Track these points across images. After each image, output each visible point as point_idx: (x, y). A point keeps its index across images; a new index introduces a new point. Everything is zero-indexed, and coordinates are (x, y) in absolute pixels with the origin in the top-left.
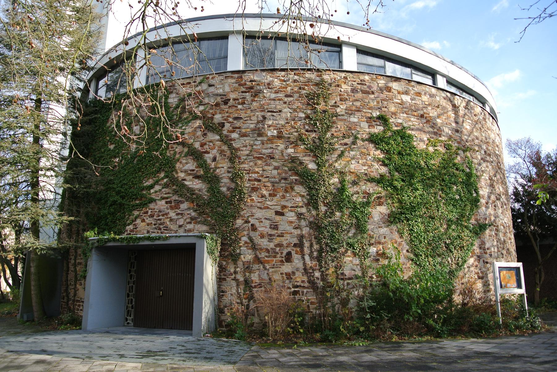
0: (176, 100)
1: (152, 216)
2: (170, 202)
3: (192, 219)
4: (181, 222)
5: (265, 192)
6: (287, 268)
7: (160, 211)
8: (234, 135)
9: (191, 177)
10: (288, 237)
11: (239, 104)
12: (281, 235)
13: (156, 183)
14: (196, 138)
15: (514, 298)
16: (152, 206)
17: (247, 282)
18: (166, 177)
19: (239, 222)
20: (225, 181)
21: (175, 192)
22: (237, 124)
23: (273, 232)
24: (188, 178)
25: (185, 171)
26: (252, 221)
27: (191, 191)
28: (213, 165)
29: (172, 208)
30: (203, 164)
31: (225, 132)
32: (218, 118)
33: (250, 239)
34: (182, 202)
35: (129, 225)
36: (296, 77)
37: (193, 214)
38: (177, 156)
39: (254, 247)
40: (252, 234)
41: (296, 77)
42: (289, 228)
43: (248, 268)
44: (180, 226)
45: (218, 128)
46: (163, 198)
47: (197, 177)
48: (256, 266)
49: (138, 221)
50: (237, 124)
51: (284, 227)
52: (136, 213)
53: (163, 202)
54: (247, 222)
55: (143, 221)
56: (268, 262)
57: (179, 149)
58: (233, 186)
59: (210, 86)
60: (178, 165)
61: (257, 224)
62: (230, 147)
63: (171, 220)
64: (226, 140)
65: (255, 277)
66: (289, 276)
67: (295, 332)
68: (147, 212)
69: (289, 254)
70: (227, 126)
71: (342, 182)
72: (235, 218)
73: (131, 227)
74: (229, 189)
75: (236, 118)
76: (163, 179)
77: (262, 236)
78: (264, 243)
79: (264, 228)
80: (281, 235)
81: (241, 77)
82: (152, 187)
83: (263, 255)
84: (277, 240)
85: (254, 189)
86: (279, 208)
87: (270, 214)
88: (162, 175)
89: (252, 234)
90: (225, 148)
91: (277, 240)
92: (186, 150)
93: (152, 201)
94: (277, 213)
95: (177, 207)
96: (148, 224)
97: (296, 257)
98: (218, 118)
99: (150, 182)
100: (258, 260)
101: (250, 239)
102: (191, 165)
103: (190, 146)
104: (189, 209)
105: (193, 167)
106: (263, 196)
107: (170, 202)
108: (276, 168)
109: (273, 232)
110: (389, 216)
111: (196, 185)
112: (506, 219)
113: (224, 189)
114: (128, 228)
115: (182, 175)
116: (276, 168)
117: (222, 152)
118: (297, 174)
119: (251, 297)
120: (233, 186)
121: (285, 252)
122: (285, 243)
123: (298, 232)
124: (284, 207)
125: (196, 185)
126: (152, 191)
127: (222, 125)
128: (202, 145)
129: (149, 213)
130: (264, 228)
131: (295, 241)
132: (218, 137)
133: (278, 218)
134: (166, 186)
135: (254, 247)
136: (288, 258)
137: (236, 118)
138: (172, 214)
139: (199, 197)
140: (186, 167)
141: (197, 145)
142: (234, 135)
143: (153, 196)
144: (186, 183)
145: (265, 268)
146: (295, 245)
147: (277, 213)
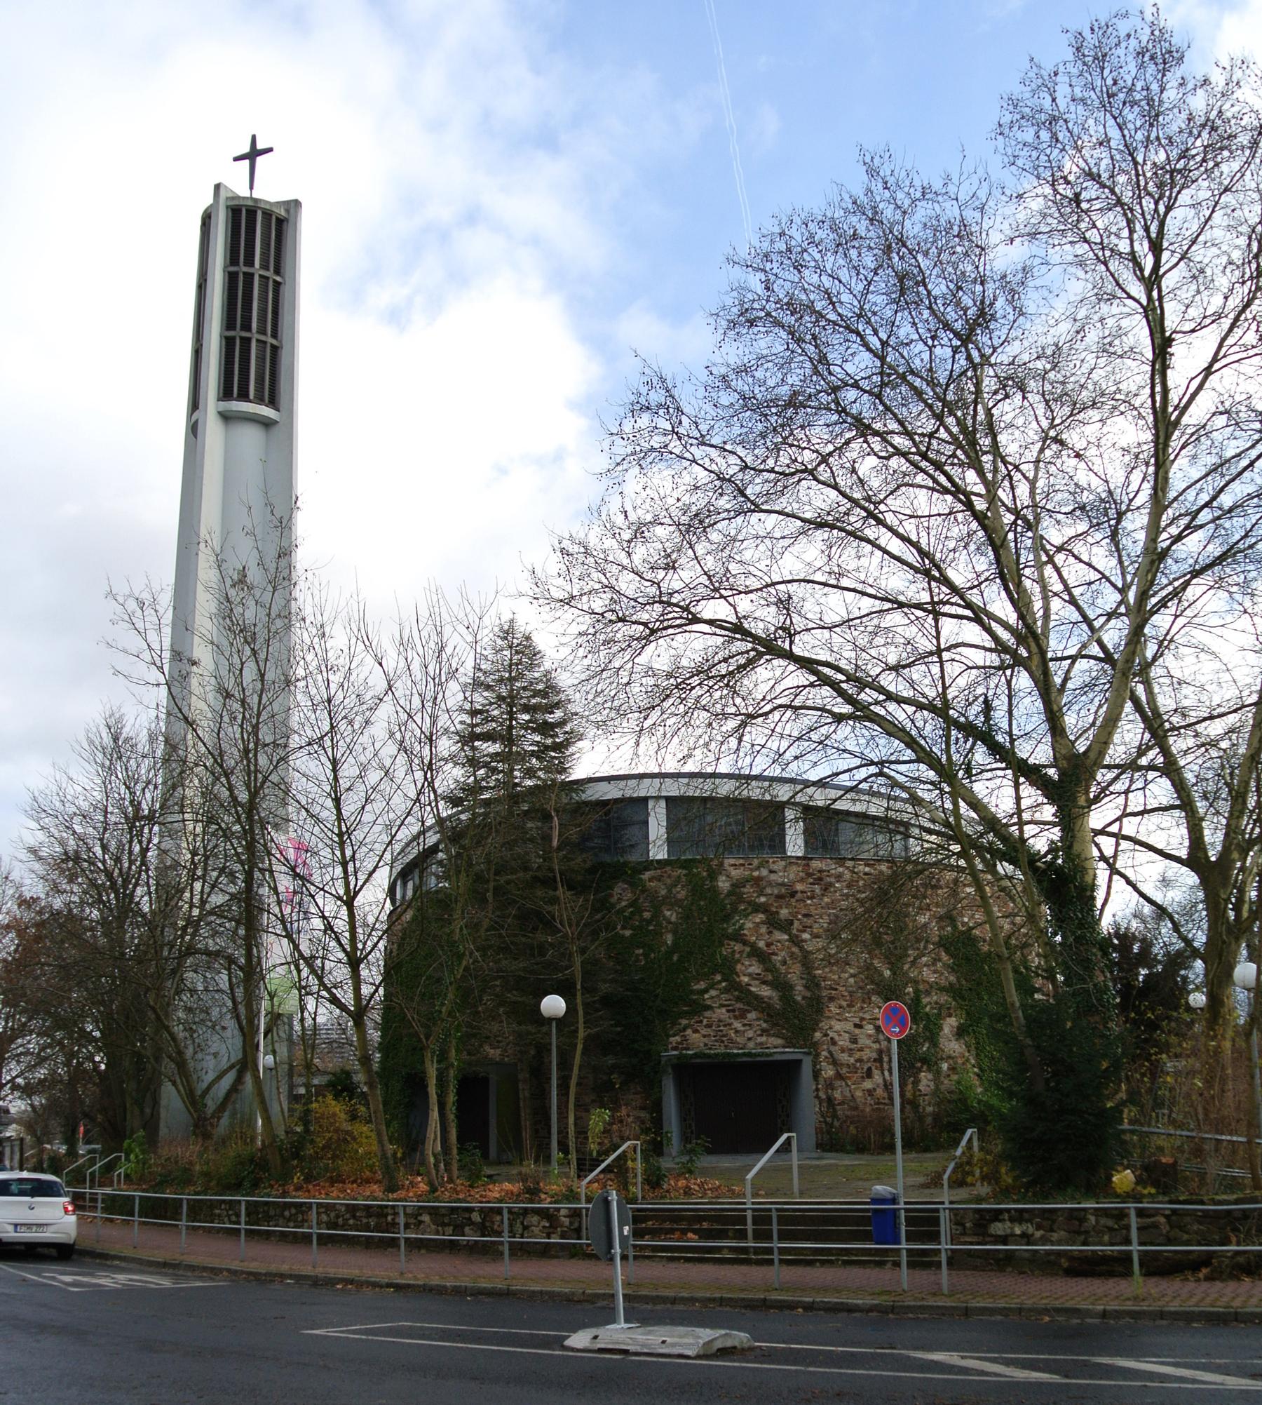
0: (727, 884)
1: (708, 1026)
2: (733, 1011)
3: (764, 1031)
4: (750, 1034)
5: (844, 1004)
6: (868, 1084)
7: (720, 1021)
8: (806, 936)
9: (757, 982)
10: (867, 1051)
11: (808, 898)
12: (861, 1050)
13: (712, 986)
14: (759, 936)
15: (928, 999)
16: (708, 1014)
17: (830, 1100)
18: (724, 980)
19: (818, 1035)
20: (799, 988)
21: (738, 999)
22: (808, 921)
23: (854, 1046)
24: (753, 982)
25: (750, 975)
26: (831, 1034)
27: (757, 997)
28: (783, 969)
29: (736, 1018)
30: (769, 968)
31: (795, 931)
32: (784, 912)
33: (830, 1052)
34: (749, 1012)
35: (674, 1035)
36: (867, 869)
37: (764, 1025)
38: (737, 956)
39: (835, 1062)
40: (833, 1048)
41: (867, 869)
42: (868, 1042)
43: (830, 1085)
44: (750, 1039)
45: (786, 926)
46: (722, 1006)
47: (764, 983)
48: (838, 1083)
49: (689, 1032)
50: (808, 921)
51: (864, 1041)
52: (684, 1022)
53: (724, 1010)
54: (826, 1035)
55: (696, 1031)
56: (849, 1078)
57: (738, 947)
58: (808, 994)
59: (771, 872)
60: (739, 967)
61: (836, 1038)
62: (801, 949)
63: (737, 1032)
64: (796, 941)
65: (837, 1095)
66: (870, 1092)
67: (909, 868)
68: (701, 1022)
69: (869, 1069)
70: (796, 924)
71: (917, 991)
72: (814, 1030)
73: (678, 1038)
74: (804, 998)
75: (805, 916)
76: (720, 982)
77: (843, 1051)
78: (844, 1057)
79: (844, 1042)
80: (861, 1050)
81: (808, 865)
82: (706, 991)
83: (844, 1071)
84: (858, 1055)
85: (831, 999)
86: (857, 1021)
87: (849, 1026)
88: (718, 977)
89: (833, 1048)
90: (795, 950)
91: (858, 1055)
92: (748, 949)
93: (709, 1008)
94: (856, 1026)
95: (742, 1015)
96: (704, 1036)
97: (876, 1072)
98: (784, 912)
99: (702, 985)
100: (839, 1076)
101: (830, 1052)
102: (755, 968)
103: (753, 946)
104: (758, 1019)
105: (758, 971)
106: (840, 1007)
107: (733, 1011)
108: (852, 976)
109: (854, 1046)
110: (958, 1028)
111: (766, 992)
112: (534, 833)
113: (799, 998)
114: (672, 1039)
115: (746, 979)
116: (852, 976)
117: (792, 955)
118: (872, 982)
119: (835, 1116)
120: (808, 994)
121: (866, 1068)
122: (865, 1058)
123: (876, 1046)
124: (862, 1019)
125: (766, 992)
126: (706, 996)
127: (791, 923)
128: (768, 945)
129: (705, 1022)
130: (844, 1042)
131: (874, 1055)
132: (786, 937)
133: (857, 1031)
134: (726, 990)
135: (835, 1062)
136: (869, 1074)
137: (805, 916)
138: (737, 1025)
139: (769, 1006)
140: (751, 970)
141: (761, 944)
142: (806, 936)
143: (708, 1003)
144: (753, 989)
145: (847, 1085)
146: (875, 1060)
147: (856, 1026)
